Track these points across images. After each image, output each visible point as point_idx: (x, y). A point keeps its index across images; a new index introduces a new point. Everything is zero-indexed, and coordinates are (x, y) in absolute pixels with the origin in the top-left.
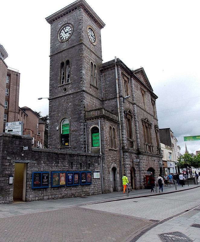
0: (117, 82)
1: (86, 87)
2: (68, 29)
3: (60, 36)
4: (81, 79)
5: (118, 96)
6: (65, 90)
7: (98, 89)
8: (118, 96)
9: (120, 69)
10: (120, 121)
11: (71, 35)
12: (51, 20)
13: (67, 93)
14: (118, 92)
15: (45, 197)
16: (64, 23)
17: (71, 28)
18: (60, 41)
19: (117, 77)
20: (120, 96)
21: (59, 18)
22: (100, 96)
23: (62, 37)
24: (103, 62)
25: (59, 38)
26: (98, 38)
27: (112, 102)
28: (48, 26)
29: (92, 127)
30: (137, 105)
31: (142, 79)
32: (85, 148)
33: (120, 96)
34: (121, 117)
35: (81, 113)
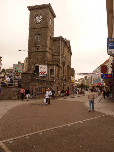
0: (61, 48)
1: (48, 49)
2: (41, 18)
3: (35, 19)
4: (46, 46)
5: (61, 55)
6: (38, 49)
7: (51, 50)
8: (61, 55)
9: (62, 42)
10: (61, 66)
11: (42, 21)
12: (31, 9)
13: (39, 51)
14: (61, 53)
15: (40, 97)
16: (38, 13)
17: (42, 17)
18: (35, 22)
19: (61, 46)
20: (62, 55)
21: (35, 9)
22: (52, 53)
23: (37, 20)
24: (54, 36)
25: (35, 20)
26: (53, 22)
27: (58, 57)
28: (28, 12)
29: (50, 69)
30: (66, 59)
31: (68, 46)
32: (47, 78)
33: (62, 55)
34: (61, 65)
35: (46, 62)
